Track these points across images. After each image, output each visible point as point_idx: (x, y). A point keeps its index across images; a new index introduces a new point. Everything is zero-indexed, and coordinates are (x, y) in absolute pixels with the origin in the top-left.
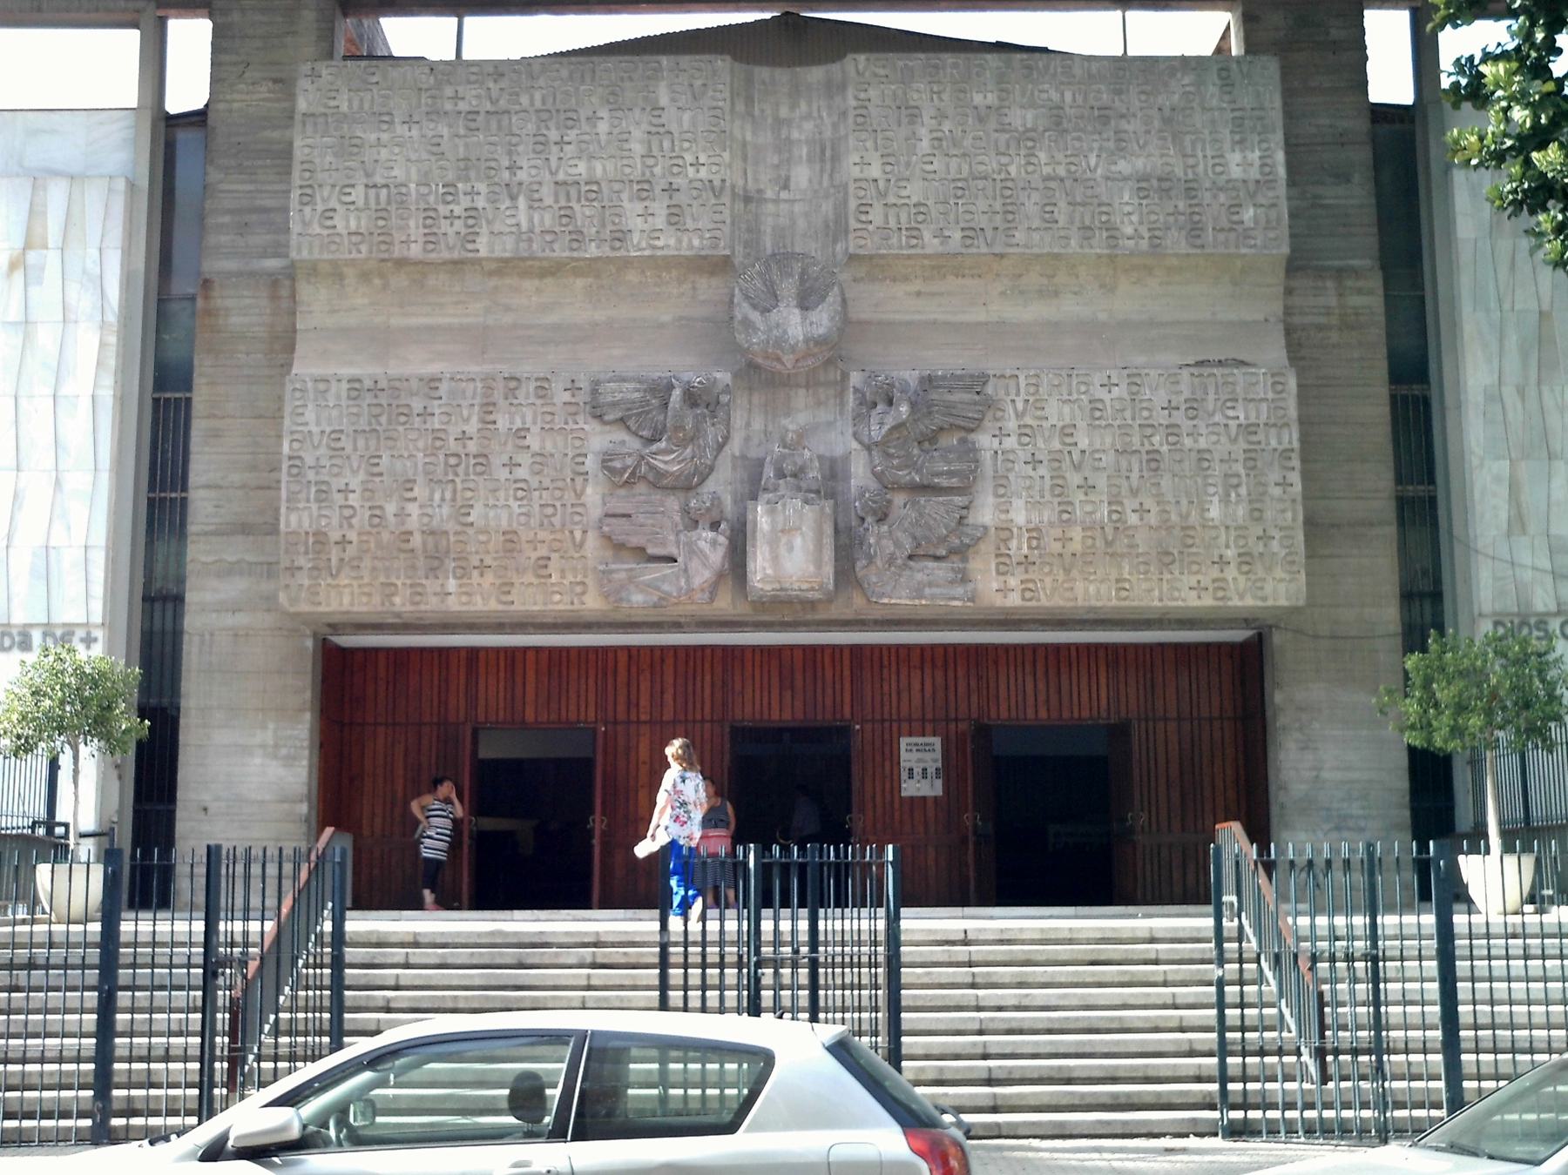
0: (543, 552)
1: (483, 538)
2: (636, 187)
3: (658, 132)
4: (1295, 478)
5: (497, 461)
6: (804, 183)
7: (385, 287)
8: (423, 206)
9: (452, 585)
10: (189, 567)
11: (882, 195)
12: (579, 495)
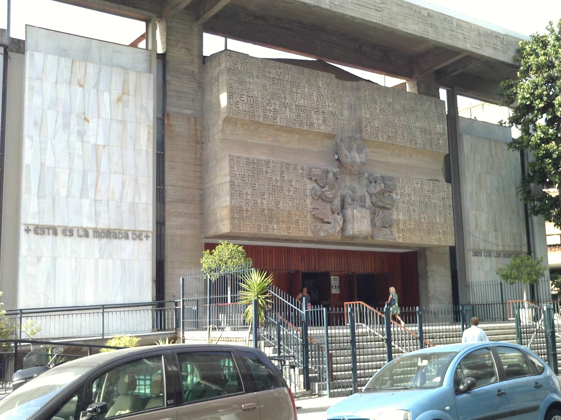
0: (297, 218)
1: (283, 212)
2: (315, 110)
3: (319, 94)
4: (452, 212)
5: (285, 189)
6: (346, 116)
7: (247, 129)
8: (262, 105)
9: (275, 226)
10: (166, 213)
11: (370, 123)
12: (305, 201)
